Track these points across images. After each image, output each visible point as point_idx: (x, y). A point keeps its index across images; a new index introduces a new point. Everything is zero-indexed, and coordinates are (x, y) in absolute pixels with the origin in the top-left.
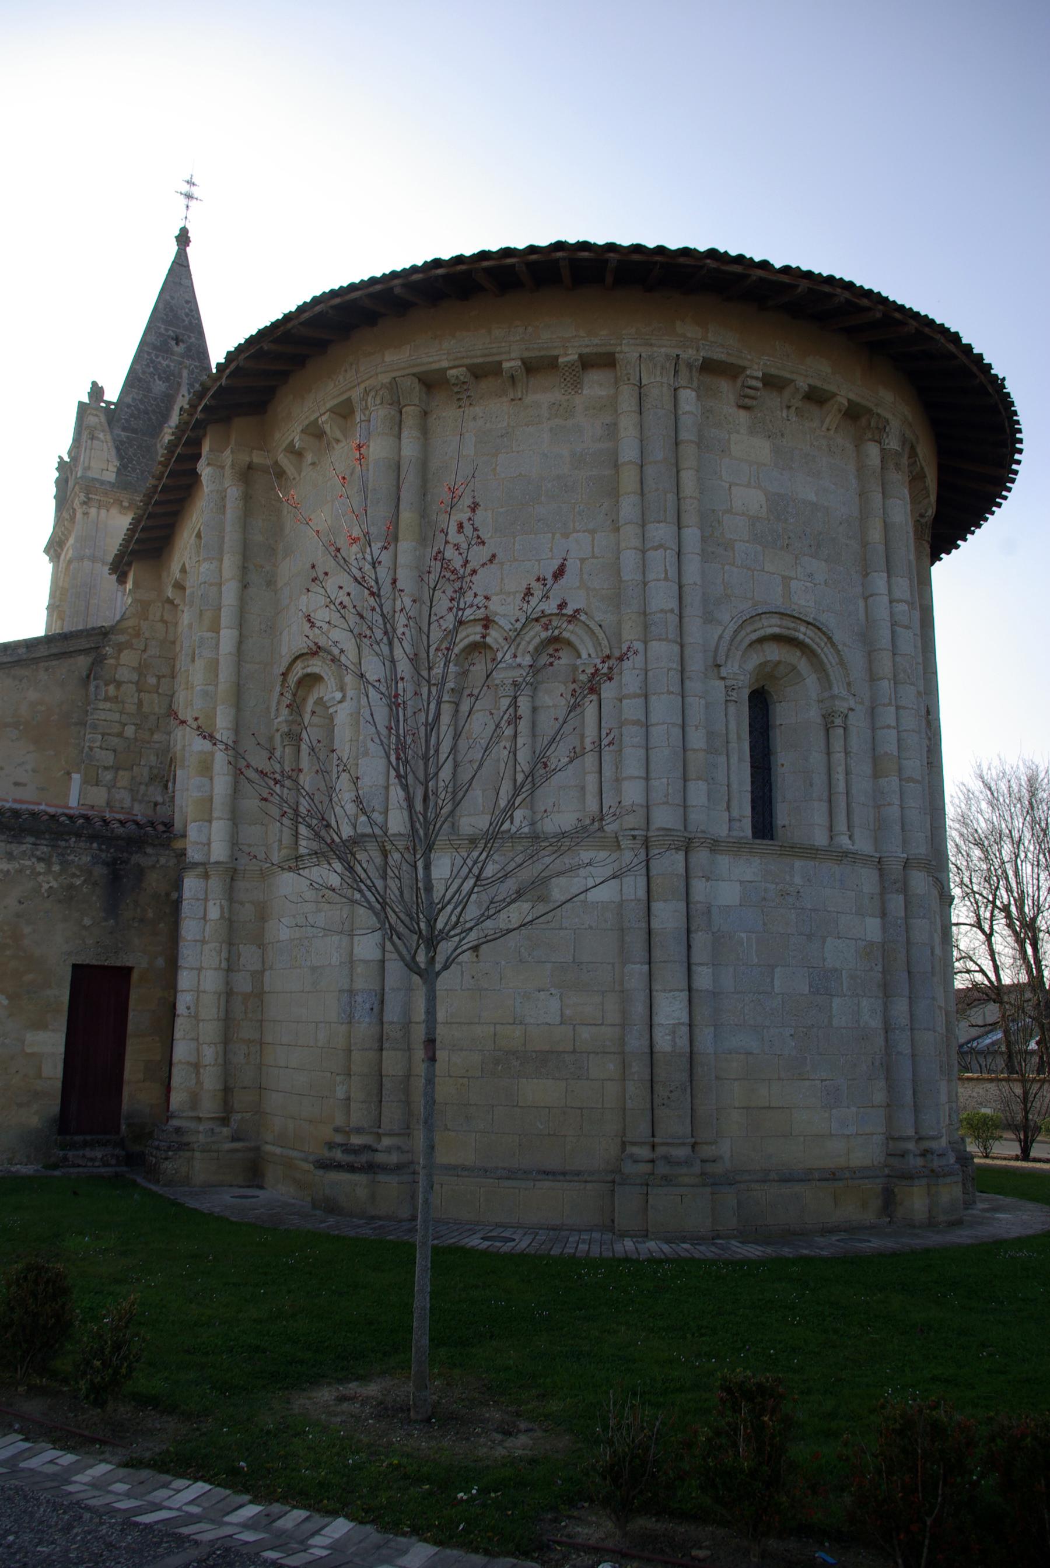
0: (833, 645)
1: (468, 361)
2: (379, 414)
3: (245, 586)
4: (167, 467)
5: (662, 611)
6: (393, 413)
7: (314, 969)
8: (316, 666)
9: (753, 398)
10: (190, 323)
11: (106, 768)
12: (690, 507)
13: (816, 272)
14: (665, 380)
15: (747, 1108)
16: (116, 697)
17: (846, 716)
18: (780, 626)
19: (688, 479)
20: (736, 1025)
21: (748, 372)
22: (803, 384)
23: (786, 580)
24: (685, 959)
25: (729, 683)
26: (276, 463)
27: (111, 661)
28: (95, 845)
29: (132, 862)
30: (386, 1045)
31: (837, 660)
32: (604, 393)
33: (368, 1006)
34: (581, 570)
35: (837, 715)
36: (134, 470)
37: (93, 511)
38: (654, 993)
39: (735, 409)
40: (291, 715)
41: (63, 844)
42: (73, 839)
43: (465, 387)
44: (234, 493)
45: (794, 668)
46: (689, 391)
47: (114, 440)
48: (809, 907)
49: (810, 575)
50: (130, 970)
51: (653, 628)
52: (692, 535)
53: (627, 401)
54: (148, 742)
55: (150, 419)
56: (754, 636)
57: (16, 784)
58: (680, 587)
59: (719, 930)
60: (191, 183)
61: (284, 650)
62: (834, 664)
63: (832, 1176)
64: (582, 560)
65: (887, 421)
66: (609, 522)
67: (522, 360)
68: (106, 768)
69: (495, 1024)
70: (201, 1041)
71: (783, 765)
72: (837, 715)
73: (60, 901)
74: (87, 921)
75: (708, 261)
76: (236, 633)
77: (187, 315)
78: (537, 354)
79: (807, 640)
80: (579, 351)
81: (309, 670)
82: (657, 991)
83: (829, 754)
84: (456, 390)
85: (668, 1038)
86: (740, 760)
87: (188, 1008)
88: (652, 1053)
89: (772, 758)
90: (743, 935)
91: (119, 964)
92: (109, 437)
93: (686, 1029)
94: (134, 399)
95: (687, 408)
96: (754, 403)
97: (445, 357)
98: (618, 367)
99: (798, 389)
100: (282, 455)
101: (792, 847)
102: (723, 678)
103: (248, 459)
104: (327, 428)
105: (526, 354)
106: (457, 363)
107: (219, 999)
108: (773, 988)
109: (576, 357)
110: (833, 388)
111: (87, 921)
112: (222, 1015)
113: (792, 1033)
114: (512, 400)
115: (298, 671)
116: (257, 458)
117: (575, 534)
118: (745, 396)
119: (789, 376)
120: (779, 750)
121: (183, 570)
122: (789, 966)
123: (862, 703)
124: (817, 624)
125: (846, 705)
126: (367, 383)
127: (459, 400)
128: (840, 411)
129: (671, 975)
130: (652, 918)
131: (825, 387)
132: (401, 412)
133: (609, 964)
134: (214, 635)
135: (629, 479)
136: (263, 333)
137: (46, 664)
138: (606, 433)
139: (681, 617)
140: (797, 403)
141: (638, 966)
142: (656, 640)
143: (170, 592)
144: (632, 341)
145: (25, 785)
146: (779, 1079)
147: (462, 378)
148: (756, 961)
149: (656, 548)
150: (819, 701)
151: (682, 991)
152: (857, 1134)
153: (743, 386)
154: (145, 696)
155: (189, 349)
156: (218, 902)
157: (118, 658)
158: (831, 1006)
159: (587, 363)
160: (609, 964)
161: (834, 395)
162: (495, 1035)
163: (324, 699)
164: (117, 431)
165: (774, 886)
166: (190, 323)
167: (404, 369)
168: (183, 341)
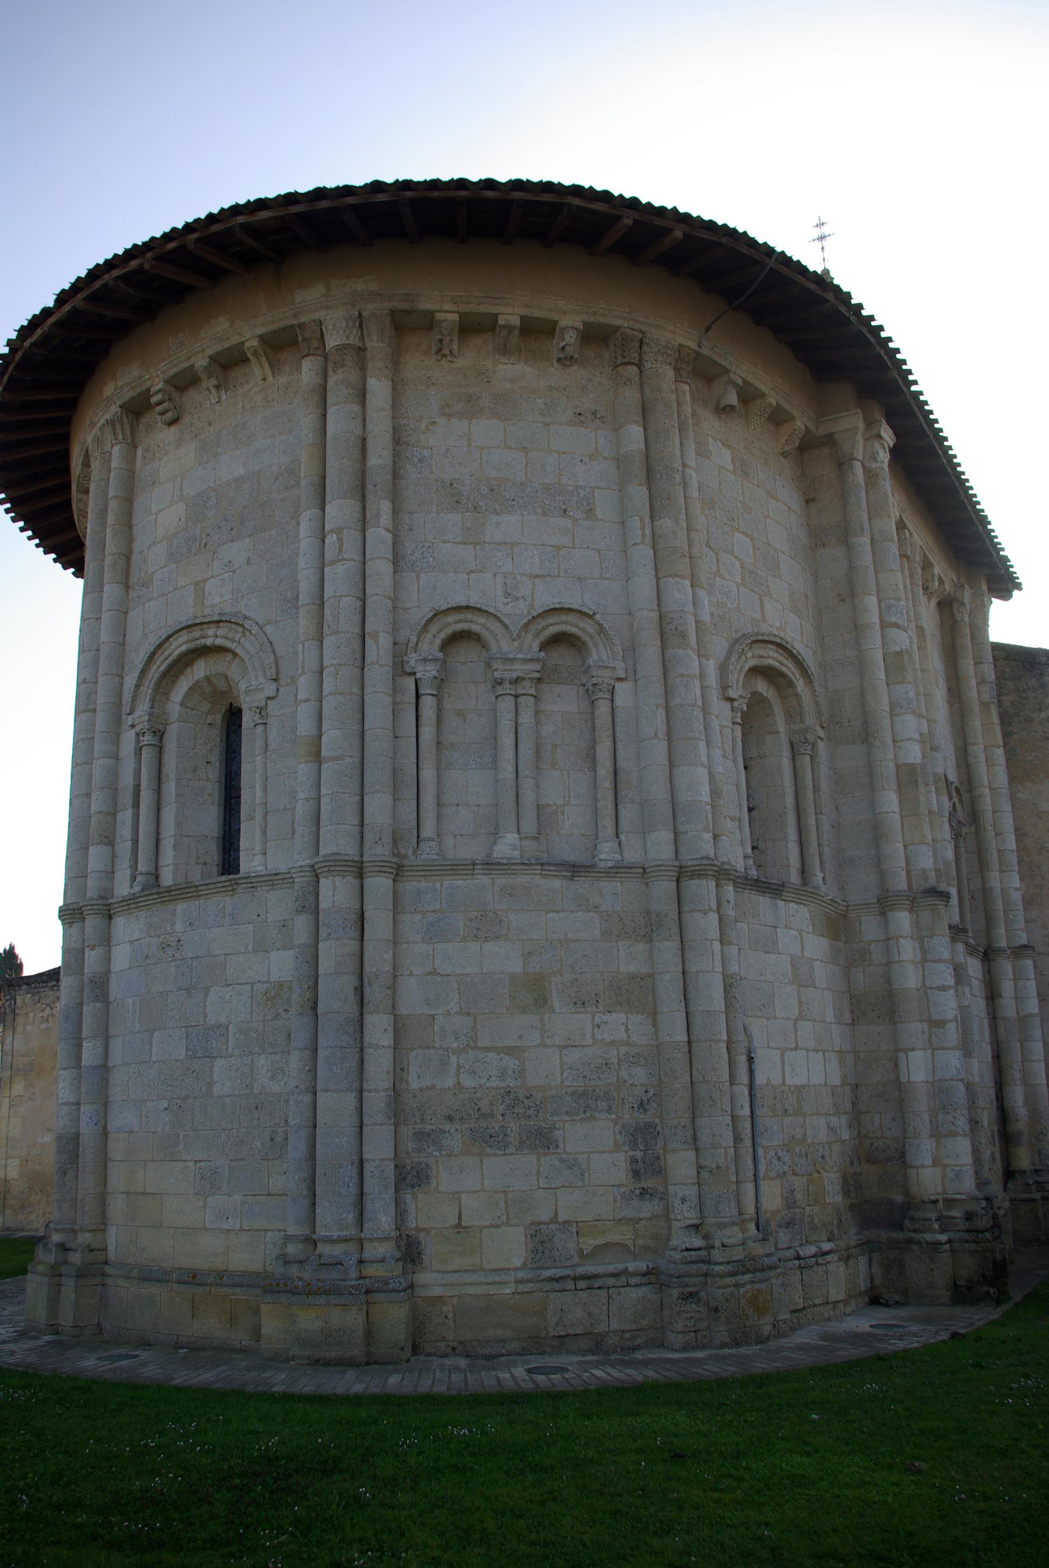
15: (128, 1193)
63: (192, 1278)
90: (130, 1000)
101: (169, 891)
108: (151, 1056)
110: (235, 340)
113: (166, 1106)
122: (166, 1028)
131: (226, 345)
148: (138, 1026)
152: (241, 1229)
165: (155, 940)
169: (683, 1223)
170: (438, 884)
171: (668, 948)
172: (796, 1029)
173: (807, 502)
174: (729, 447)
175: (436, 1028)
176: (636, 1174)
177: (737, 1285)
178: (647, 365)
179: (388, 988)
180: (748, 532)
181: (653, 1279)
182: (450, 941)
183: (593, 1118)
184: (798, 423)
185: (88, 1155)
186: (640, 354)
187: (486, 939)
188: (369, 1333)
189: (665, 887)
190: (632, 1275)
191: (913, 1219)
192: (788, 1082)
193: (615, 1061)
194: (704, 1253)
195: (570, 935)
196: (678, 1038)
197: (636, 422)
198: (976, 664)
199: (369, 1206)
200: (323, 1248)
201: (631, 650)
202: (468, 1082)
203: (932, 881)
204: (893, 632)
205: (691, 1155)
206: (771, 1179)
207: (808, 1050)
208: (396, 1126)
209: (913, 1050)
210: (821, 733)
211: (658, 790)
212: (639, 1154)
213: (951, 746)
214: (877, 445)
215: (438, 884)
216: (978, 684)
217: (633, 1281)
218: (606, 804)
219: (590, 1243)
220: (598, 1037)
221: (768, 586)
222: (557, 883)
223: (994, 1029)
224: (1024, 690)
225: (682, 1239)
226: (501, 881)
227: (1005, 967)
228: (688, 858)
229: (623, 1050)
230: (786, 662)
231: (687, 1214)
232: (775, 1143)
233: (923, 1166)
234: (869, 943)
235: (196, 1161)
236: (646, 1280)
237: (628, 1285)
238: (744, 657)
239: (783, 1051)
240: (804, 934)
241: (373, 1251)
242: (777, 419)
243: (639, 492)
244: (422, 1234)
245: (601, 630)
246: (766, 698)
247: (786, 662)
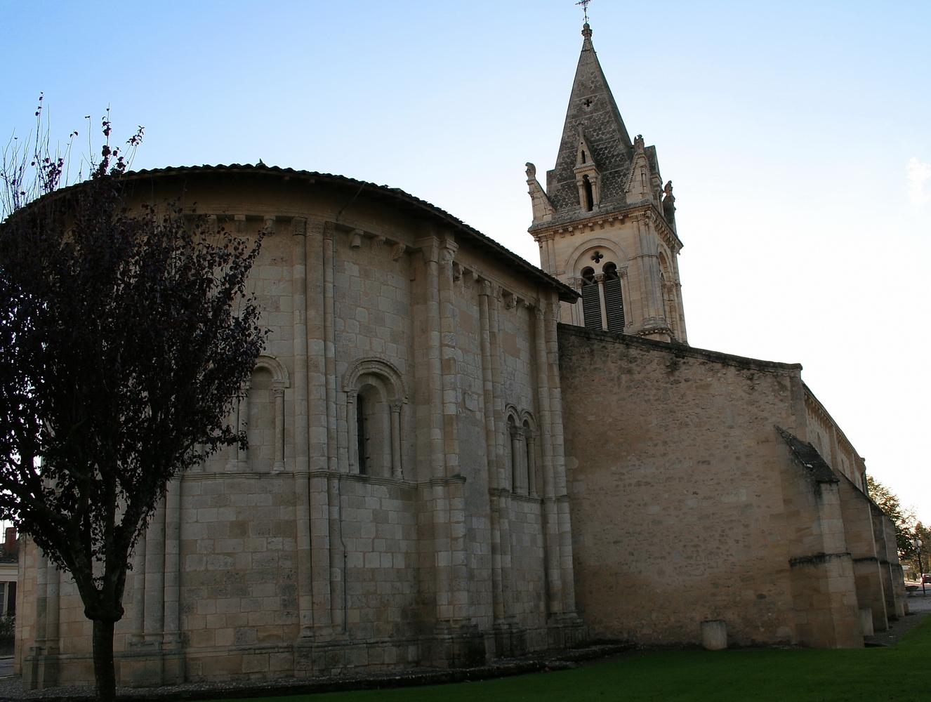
15: (68, 623)
56: (365, 371)
166: (596, 87)
168: (591, 102)
169: (304, 627)
170: (200, 483)
171: (301, 510)
172: (373, 543)
173: (411, 281)
174: (358, 264)
175: (198, 545)
176: (285, 606)
177: (325, 652)
178: (308, 234)
179: (176, 529)
180: (366, 306)
181: (290, 649)
182: (205, 508)
183: (266, 582)
184: (401, 245)
185: (51, 606)
186: (305, 229)
187: (220, 507)
188: (163, 671)
189: (301, 482)
190: (281, 648)
191: (437, 629)
192: (366, 567)
193: (277, 558)
194: (312, 639)
195: (258, 504)
196: (305, 548)
197: (300, 264)
198: (547, 342)
199: (166, 621)
200: (147, 638)
201: (291, 375)
202: (210, 568)
203: (456, 472)
204: (445, 349)
205: (309, 598)
206: (355, 609)
207: (380, 553)
208: (180, 587)
209: (440, 551)
210: (406, 401)
211: (299, 438)
212: (286, 598)
213: (529, 389)
214: (446, 253)
215: (200, 483)
216: (548, 353)
217: (281, 650)
218: (279, 445)
219: (262, 635)
220: (269, 548)
221: (376, 333)
222: (253, 481)
223: (545, 540)
224: (583, 353)
225: (304, 633)
226: (228, 481)
227: (553, 508)
228: (313, 469)
229: (280, 553)
230: (384, 369)
231: (305, 622)
232: (358, 593)
233: (442, 605)
234: (426, 501)
236: (286, 650)
237: (278, 652)
238: (357, 370)
239: (364, 553)
240: (383, 500)
241: (167, 639)
242: (390, 244)
243: (299, 298)
244: (190, 633)
245: (279, 365)
246: (375, 387)
247: (384, 369)
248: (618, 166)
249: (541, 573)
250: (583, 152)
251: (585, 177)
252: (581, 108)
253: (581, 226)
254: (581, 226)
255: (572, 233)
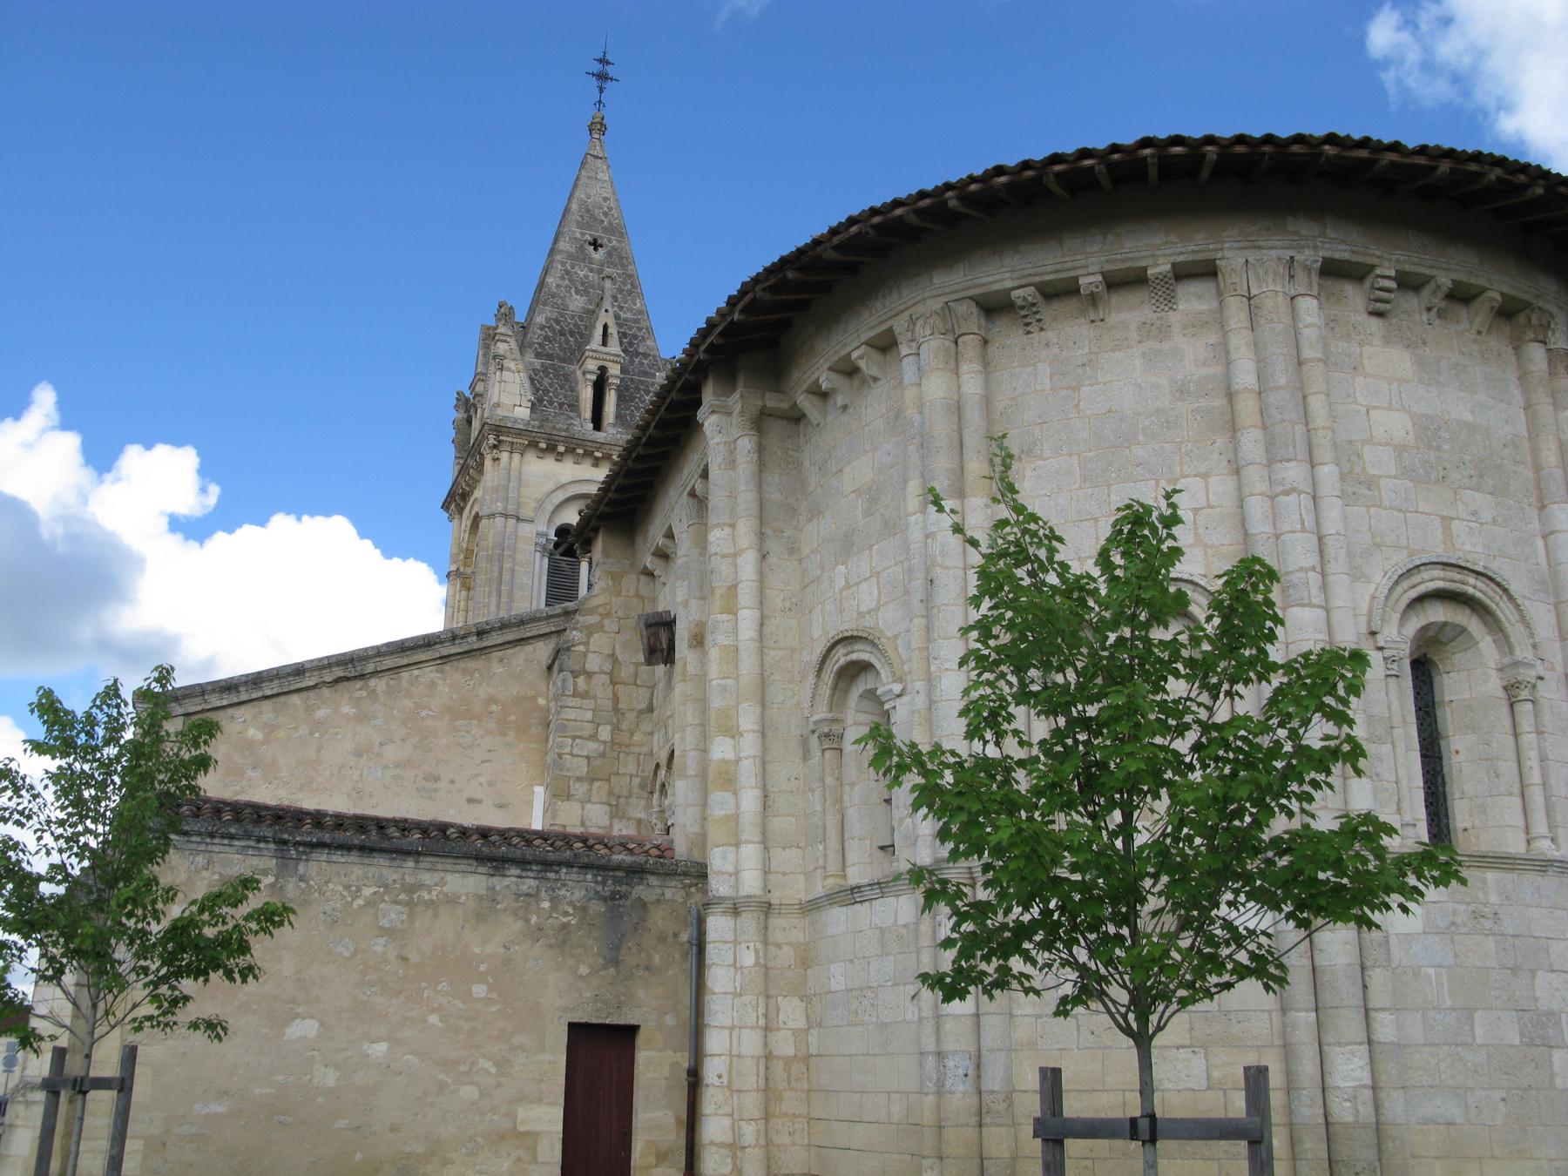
0: (1511, 598)
1: (1037, 279)
2: (932, 347)
3: (764, 557)
4: (654, 415)
5: (1301, 569)
6: (947, 343)
7: (883, 1026)
8: (862, 654)
9: (1387, 302)
10: (610, 224)
11: (579, 779)
12: (1322, 439)
13: (1459, 149)
14: (1279, 288)
16: (587, 692)
17: (1534, 686)
18: (1443, 579)
19: (1317, 403)
20: (1431, 1087)
21: (1378, 271)
22: (1445, 281)
23: (1446, 520)
24: (1362, 1004)
25: (1387, 653)
26: (795, 405)
27: (581, 648)
28: (589, 877)
29: (634, 895)
30: (987, 1120)
31: (1517, 616)
32: (1204, 307)
33: (961, 1072)
34: (1195, 523)
35: (1522, 687)
36: (551, 403)
37: (505, 456)
38: (1326, 1048)
39: (1365, 316)
40: (831, 711)
41: (552, 875)
42: (564, 870)
43: (1034, 309)
44: (746, 444)
45: (1463, 630)
46: (1309, 298)
47: (526, 369)
48: (1511, 932)
49: (1474, 513)
50: (632, 1031)
51: (1291, 591)
52: (1328, 473)
53: (1236, 311)
54: (627, 746)
55: (567, 341)
56: (1413, 594)
57: (470, 801)
58: (1320, 539)
59: (1399, 966)
60: (604, 61)
61: (817, 633)
62: (1513, 621)
64: (1196, 511)
65: (1552, 316)
66: (1225, 463)
67: (1103, 274)
68: (579, 779)
69: (1124, 1091)
70: (736, 1117)
71: (1457, 752)
72: (1522, 687)
73: (551, 946)
74: (584, 970)
75: (1327, 147)
76: (757, 614)
77: (606, 214)
78: (1122, 266)
79: (1478, 595)
80: (1172, 259)
81: (854, 657)
82: (1329, 1045)
83: (1516, 735)
84: (1023, 313)
85: (1348, 1104)
86: (1408, 749)
87: (720, 1077)
88: (1327, 1123)
89: (1442, 743)
90: (1431, 971)
91: (622, 1022)
92: (521, 366)
93: (1368, 1093)
94: (548, 320)
95: (1309, 320)
96: (1388, 306)
97: (1008, 275)
98: (1220, 276)
99: (1438, 287)
100: (802, 397)
102: (1381, 649)
103: (760, 403)
104: (862, 364)
105: (1108, 267)
106: (1023, 282)
107: (758, 1065)
108: (1474, 1038)
109: (1168, 267)
111: (584, 970)
112: (762, 1084)
113: (1504, 1095)
114: (1093, 321)
115: (841, 657)
116: (772, 401)
117: (1183, 480)
118: (1378, 300)
119: (1427, 272)
120: (1451, 733)
121: (670, 535)
123: (1553, 669)
124: (1490, 573)
125: (1534, 673)
126: (912, 311)
127: (1028, 324)
128: (1492, 308)
129: (1347, 1023)
130: (1316, 952)
132: (956, 343)
133: (1263, 1011)
134: (730, 617)
135: (1247, 407)
136: (784, 262)
137: (501, 653)
138: (1212, 354)
139: (1323, 574)
140: (1438, 301)
141: (1303, 1014)
142: (1297, 605)
143: (649, 561)
144: (1235, 245)
145: (480, 802)
146: (1493, 1157)
147: (1030, 298)
149: (1287, 493)
150: (1501, 670)
151: (1361, 1044)
153: (1373, 288)
154: (620, 688)
155: (610, 254)
156: (752, 945)
157: (587, 644)
158: (1551, 1062)
159: (1183, 273)
160: (1263, 1011)
161: (1483, 290)
162: (1124, 1105)
163: (879, 692)
164: (530, 357)
165: (1464, 907)
166: (610, 224)
167: (957, 291)
168: (601, 246)
235: (1551, 1160)
248: (645, 374)
249: (1518, 719)
250: (605, 327)
251: (603, 369)
252: (582, 249)
253: (580, 451)
254: (580, 451)
255: (560, 457)
